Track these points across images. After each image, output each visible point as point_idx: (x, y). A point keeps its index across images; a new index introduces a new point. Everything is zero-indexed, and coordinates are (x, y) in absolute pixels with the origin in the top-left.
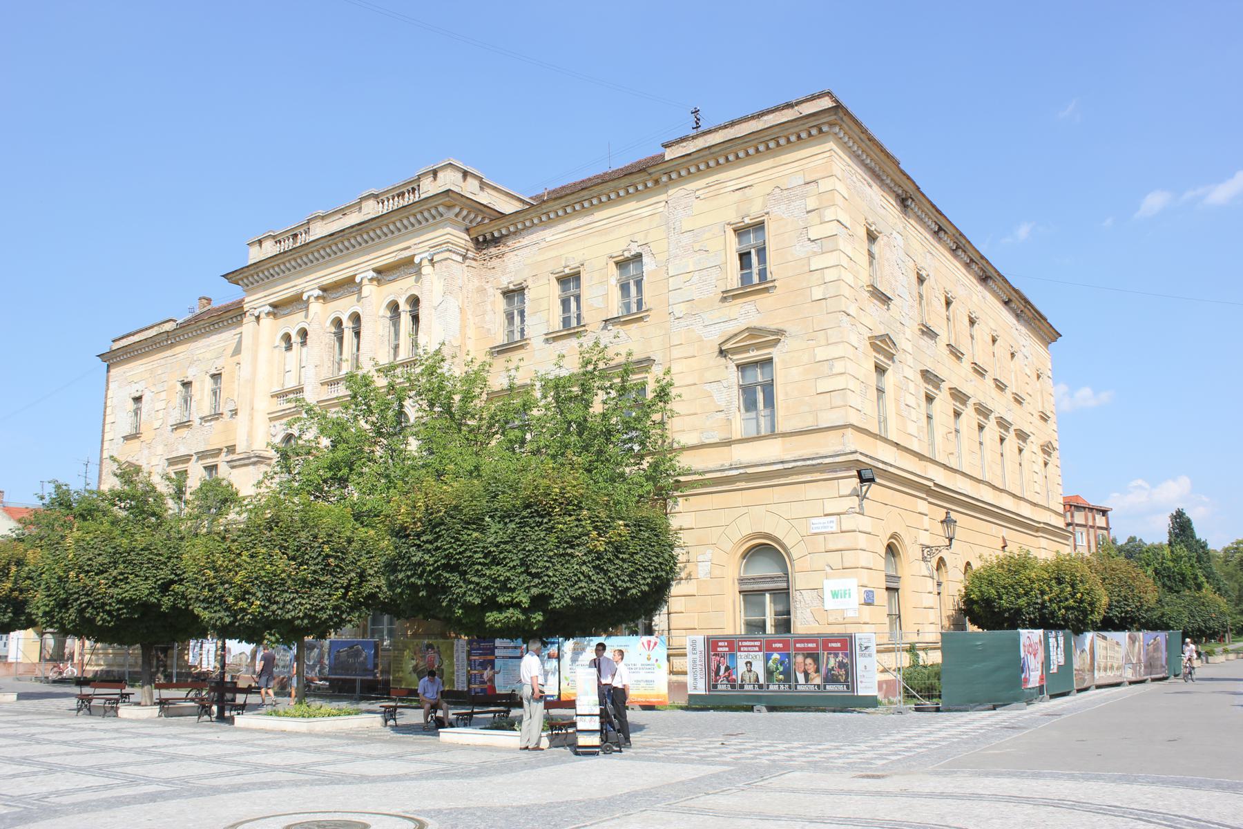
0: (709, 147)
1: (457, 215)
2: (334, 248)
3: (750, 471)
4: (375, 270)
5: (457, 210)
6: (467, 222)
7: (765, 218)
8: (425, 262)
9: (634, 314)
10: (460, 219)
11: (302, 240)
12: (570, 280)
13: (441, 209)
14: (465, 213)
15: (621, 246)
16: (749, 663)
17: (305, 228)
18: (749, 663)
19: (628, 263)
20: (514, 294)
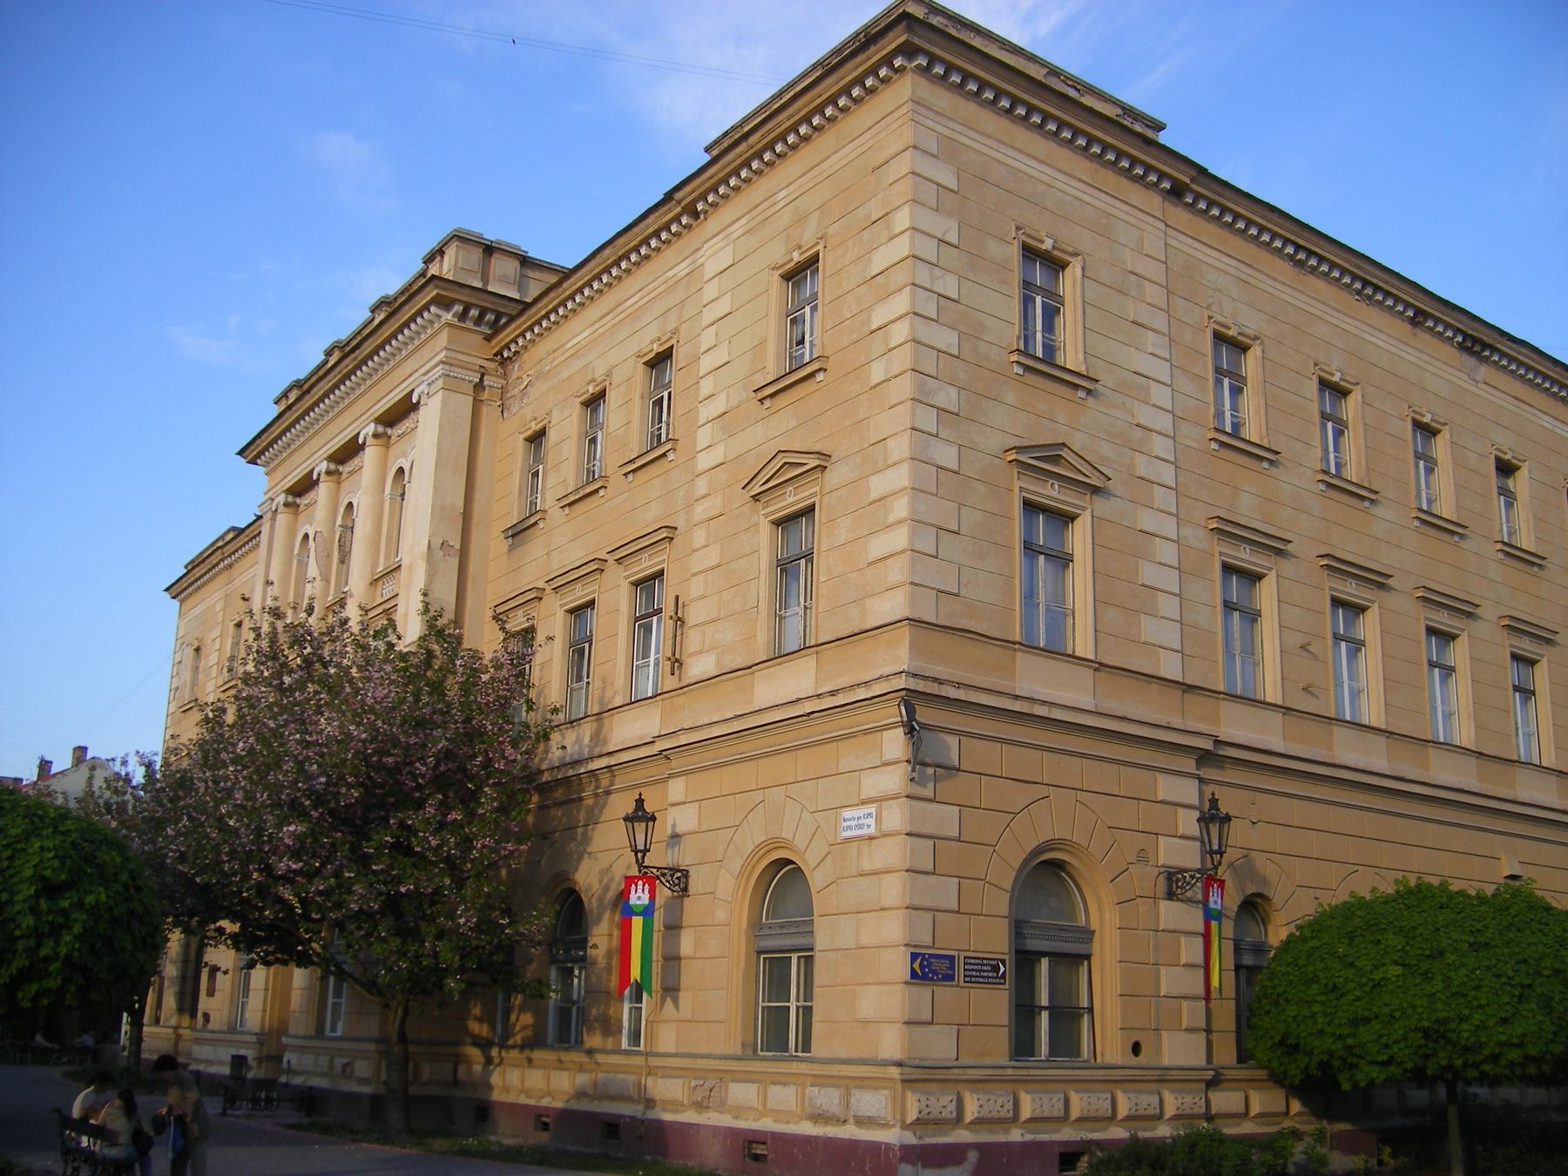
15: (648, 341)
19: (659, 361)
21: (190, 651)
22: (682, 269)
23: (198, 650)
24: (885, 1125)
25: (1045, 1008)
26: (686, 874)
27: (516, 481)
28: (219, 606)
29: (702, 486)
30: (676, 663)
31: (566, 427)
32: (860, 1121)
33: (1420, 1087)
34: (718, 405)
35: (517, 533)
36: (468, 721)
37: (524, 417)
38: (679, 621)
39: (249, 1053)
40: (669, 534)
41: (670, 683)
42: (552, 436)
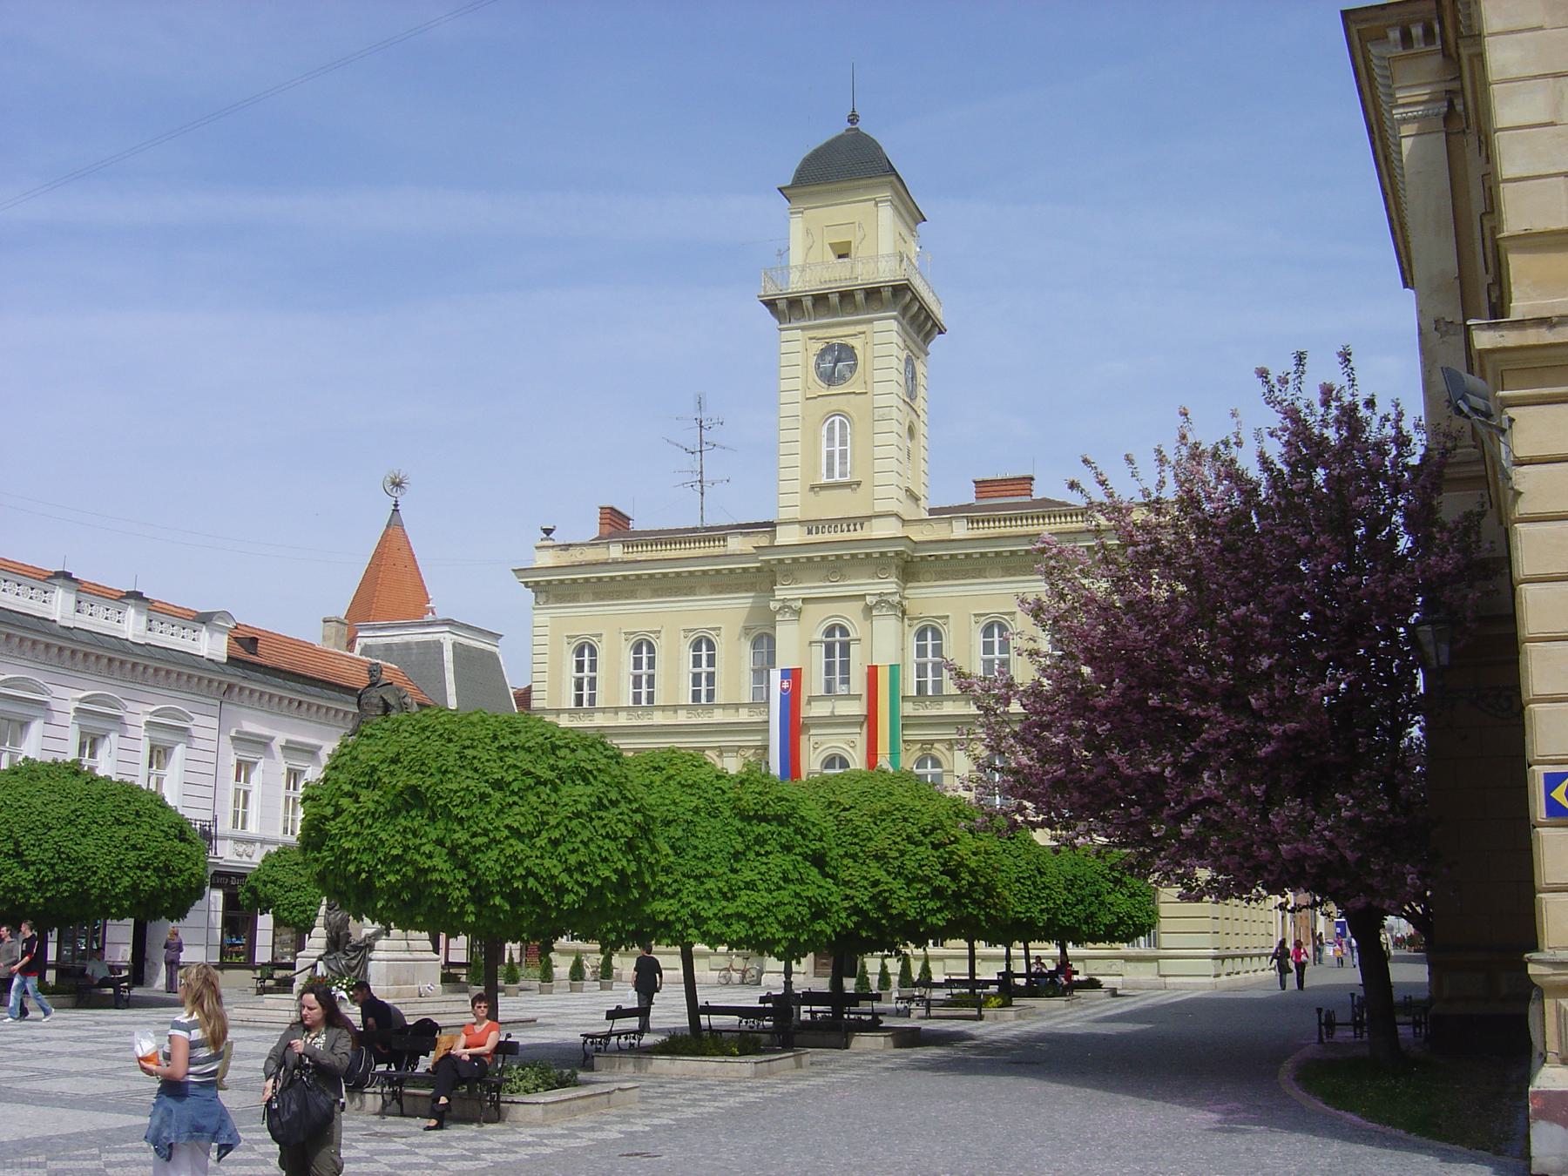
5: (1395, 35)
10: (1420, 47)
14: (1417, 31)
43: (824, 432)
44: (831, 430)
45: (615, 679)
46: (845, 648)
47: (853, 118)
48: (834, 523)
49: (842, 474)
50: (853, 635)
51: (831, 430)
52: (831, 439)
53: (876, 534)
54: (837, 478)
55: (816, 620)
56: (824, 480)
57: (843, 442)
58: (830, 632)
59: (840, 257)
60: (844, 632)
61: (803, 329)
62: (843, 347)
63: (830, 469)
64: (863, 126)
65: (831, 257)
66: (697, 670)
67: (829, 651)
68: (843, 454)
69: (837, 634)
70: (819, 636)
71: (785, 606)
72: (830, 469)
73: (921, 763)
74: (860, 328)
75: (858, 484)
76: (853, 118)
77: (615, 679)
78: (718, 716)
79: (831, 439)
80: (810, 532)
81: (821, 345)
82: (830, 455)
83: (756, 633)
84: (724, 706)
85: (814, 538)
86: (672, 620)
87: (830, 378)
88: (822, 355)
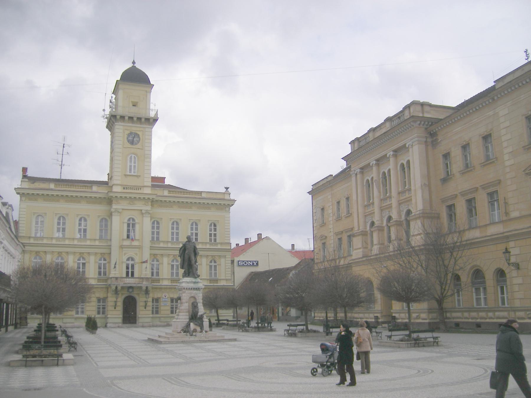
0: (510, 82)
1: (419, 124)
2: (405, 127)
3: (473, 241)
4: (393, 151)
5: (419, 122)
6: (425, 126)
7: (491, 132)
8: (410, 146)
9: (488, 161)
10: (421, 126)
11: (402, 119)
12: (465, 147)
13: (412, 123)
14: (423, 123)
15: (483, 130)
16: (131, 225)
17: (402, 114)
18: (131, 225)
19: (487, 138)
20: (446, 156)
21: (319, 210)
22: (491, 113)
23: (323, 209)
24: (404, 319)
25: (346, 315)
26: (518, 264)
27: (441, 166)
28: (329, 197)
29: (508, 170)
30: (507, 214)
31: (456, 153)
32: (472, 318)
33: (395, 317)
34: (510, 149)
35: (445, 180)
36: (397, 251)
37: (443, 148)
38: (506, 203)
39: (379, 315)
40: (499, 182)
41: (505, 218)
42: (452, 155)
43: (129, 159)
44: (131, 158)
45: (73, 229)
46: (134, 225)
47: (134, 63)
48: (132, 187)
49: (134, 172)
50: (137, 221)
51: (131, 158)
52: (131, 161)
53: (145, 192)
54: (132, 173)
55: (126, 216)
56: (128, 173)
57: (135, 163)
58: (129, 220)
59: (134, 106)
60: (133, 220)
61: (123, 126)
62: (136, 134)
63: (130, 170)
64: (137, 66)
65: (131, 105)
66: (59, 227)
67: (128, 225)
68: (135, 166)
69: (131, 220)
70: (126, 221)
71: (117, 211)
72: (130, 170)
73: (57, 259)
74: (141, 129)
75: (140, 176)
76: (134, 63)
77: (73, 229)
78: (88, 243)
79: (131, 161)
80: (124, 189)
81: (128, 132)
82: (131, 166)
83: (101, 217)
84: (90, 240)
85: (125, 191)
86: (74, 210)
87: (132, 143)
88: (129, 135)
